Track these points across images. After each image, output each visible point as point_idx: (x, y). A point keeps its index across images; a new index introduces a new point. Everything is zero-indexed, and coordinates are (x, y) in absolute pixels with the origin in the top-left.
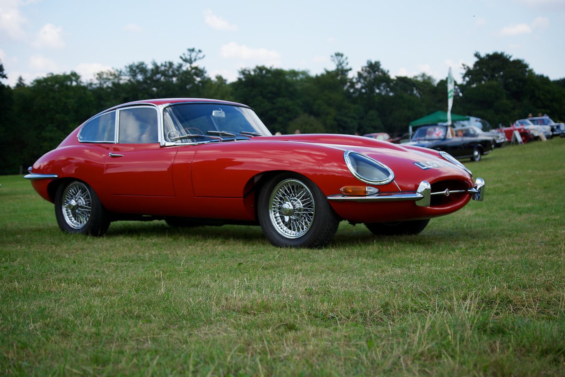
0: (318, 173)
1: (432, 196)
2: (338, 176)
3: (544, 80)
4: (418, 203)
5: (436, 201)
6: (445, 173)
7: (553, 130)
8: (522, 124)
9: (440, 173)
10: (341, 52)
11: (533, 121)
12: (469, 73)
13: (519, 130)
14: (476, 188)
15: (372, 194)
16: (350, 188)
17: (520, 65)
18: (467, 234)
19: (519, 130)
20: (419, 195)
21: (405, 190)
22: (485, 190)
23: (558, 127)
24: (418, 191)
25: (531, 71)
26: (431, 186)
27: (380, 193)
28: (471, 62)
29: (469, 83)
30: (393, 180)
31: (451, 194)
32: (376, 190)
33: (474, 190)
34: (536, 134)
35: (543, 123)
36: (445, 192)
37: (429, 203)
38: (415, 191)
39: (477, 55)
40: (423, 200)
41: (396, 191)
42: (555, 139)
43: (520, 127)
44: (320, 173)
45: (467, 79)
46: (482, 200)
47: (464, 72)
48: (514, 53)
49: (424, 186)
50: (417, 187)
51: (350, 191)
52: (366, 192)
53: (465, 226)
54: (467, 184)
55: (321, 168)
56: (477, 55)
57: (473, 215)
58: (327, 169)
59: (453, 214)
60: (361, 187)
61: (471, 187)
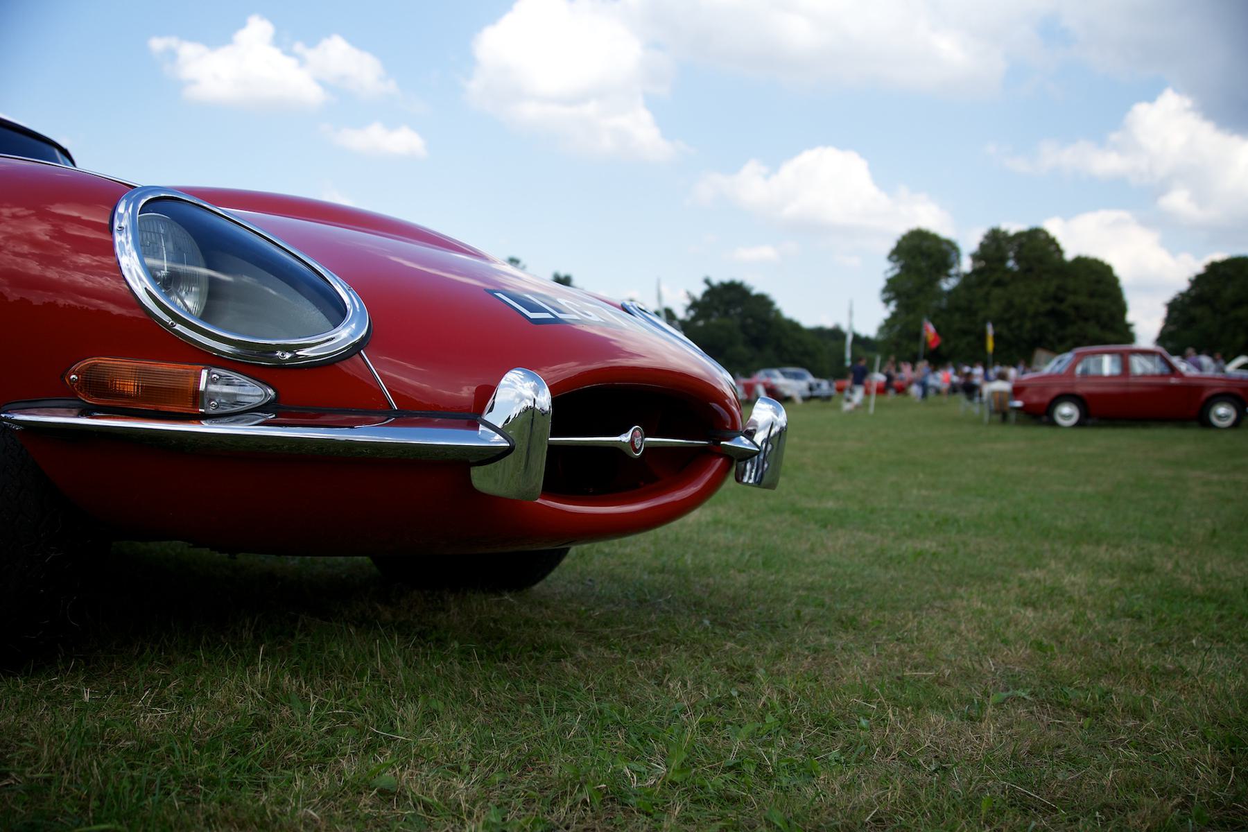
0: (37, 298)
1: (553, 448)
2: (120, 316)
3: (794, 326)
4: (483, 479)
5: (572, 473)
6: (632, 355)
7: (811, 388)
8: (768, 376)
9: (615, 351)
10: (516, 255)
11: (784, 374)
12: (695, 305)
13: (765, 384)
14: (750, 435)
15: (234, 412)
16: (127, 372)
17: (763, 302)
18: (698, 604)
19: (765, 384)
20: (497, 440)
21: (413, 410)
22: (787, 452)
23: (819, 385)
24: (488, 417)
25: (778, 313)
26: (555, 402)
27: (278, 410)
28: (699, 291)
29: (694, 319)
30: (356, 348)
31: (650, 450)
32: (253, 392)
33: (743, 443)
34: (788, 392)
35: (797, 377)
36: (625, 438)
37: (538, 480)
38: (472, 415)
39: (707, 281)
40: (510, 458)
41: (367, 405)
42: (814, 403)
43: (765, 379)
44: (48, 297)
45: (692, 313)
46: (772, 486)
47: (688, 302)
48: (757, 285)
49: (520, 393)
50: (485, 394)
51: (130, 387)
52: (198, 397)
53: (688, 558)
54: (716, 413)
55: (52, 274)
56: (707, 281)
57: (708, 524)
58: (79, 278)
59: (660, 531)
60: (165, 370)
61: (734, 432)
